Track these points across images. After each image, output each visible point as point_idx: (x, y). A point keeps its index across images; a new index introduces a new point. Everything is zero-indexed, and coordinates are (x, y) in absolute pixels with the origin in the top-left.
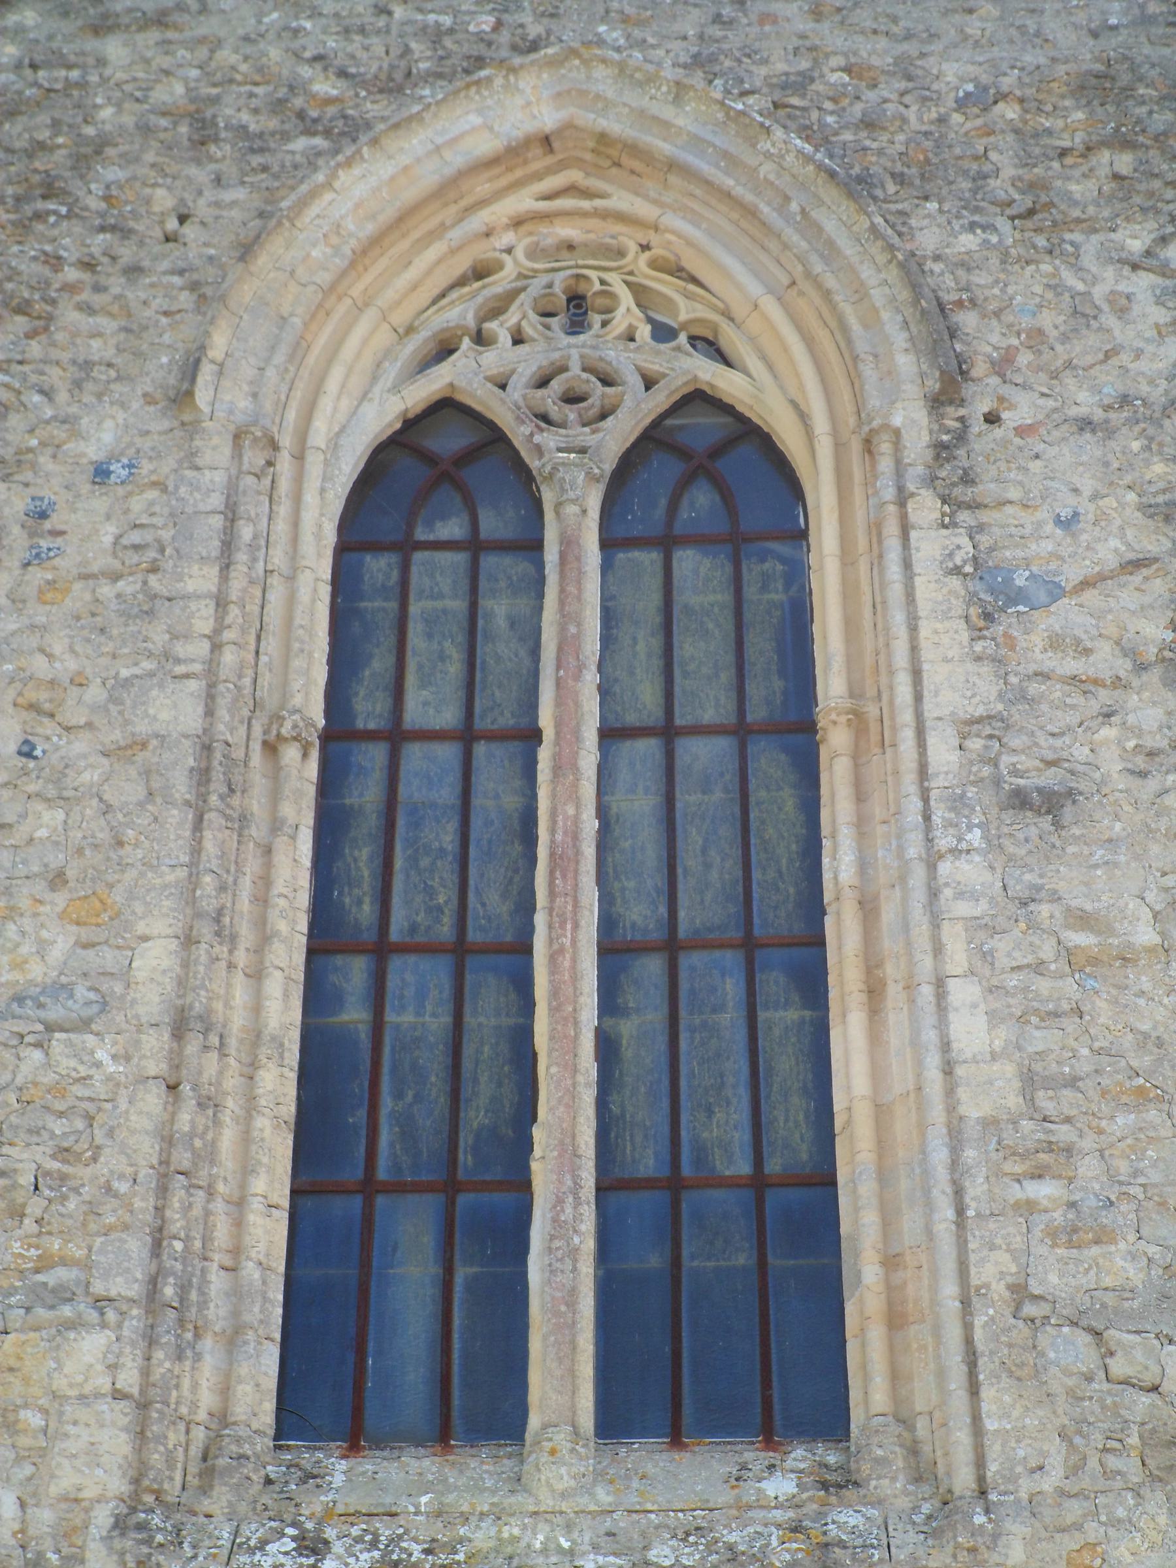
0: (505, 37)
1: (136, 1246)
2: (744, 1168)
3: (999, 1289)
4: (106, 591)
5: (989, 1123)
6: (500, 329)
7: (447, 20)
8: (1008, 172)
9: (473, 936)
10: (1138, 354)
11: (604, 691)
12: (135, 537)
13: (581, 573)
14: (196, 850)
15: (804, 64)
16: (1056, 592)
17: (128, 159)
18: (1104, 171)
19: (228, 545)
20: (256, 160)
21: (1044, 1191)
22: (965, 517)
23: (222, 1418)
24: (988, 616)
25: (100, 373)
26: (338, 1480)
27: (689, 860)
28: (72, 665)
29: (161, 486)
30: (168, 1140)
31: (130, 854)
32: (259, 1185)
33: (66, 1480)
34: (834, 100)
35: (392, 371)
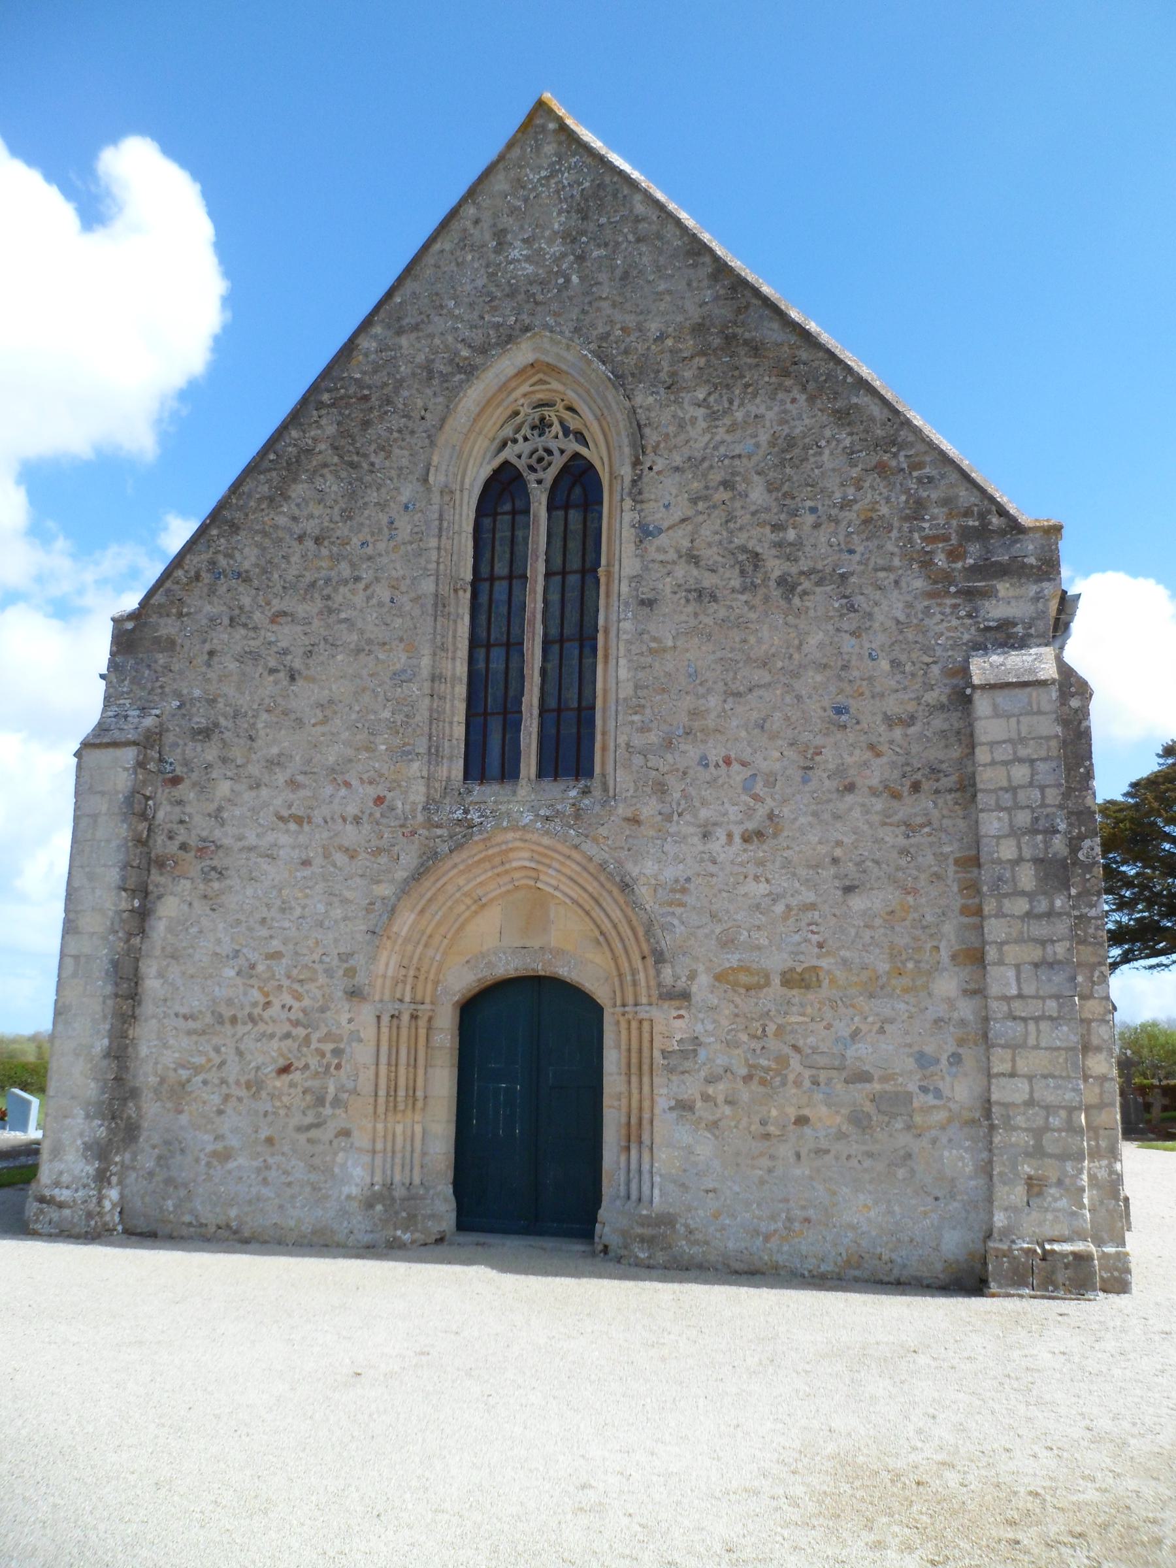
0: (518, 326)
1: (425, 740)
2: (576, 705)
3: (623, 745)
4: (409, 548)
5: (625, 699)
6: (519, 437)
7: (501, 320)
8: (666, 369)
9: (512, 641)
10: (696, 441)
11: (547, 561)
12: (416, 530)
13: (538, 525)
14: (435, 628)
15: (608, 328)
16: (660, 531)
17: (409, 387)
18: (695, 367)
19: (440, 529)
20: (445, 385)
21: (636, 718)
22: (638, 507)
23: (449, 779)
24: (641, 541)
25: (405, 471)
26: (475, 793)
27: (567, 614)
28: (401, 573)
29: (421, 511)
30: (431, 710)
31: (419, 631)
32: (456, 719)
33: (412, 798)
34: (616, 343)
35: (489, 455)
